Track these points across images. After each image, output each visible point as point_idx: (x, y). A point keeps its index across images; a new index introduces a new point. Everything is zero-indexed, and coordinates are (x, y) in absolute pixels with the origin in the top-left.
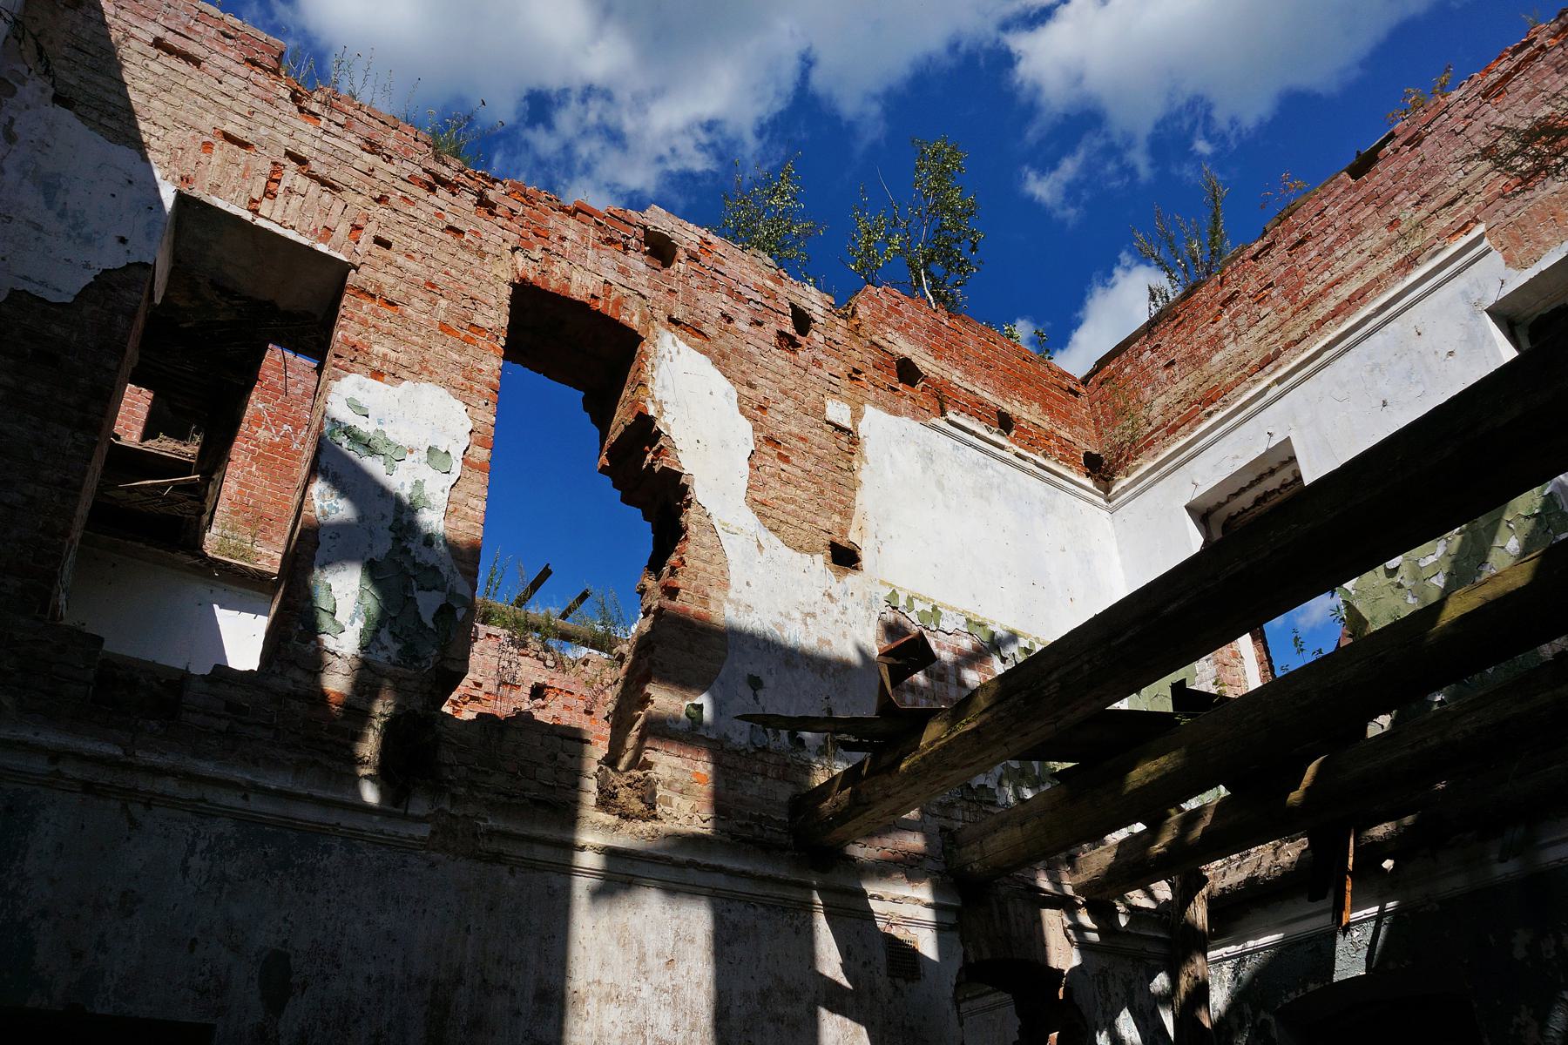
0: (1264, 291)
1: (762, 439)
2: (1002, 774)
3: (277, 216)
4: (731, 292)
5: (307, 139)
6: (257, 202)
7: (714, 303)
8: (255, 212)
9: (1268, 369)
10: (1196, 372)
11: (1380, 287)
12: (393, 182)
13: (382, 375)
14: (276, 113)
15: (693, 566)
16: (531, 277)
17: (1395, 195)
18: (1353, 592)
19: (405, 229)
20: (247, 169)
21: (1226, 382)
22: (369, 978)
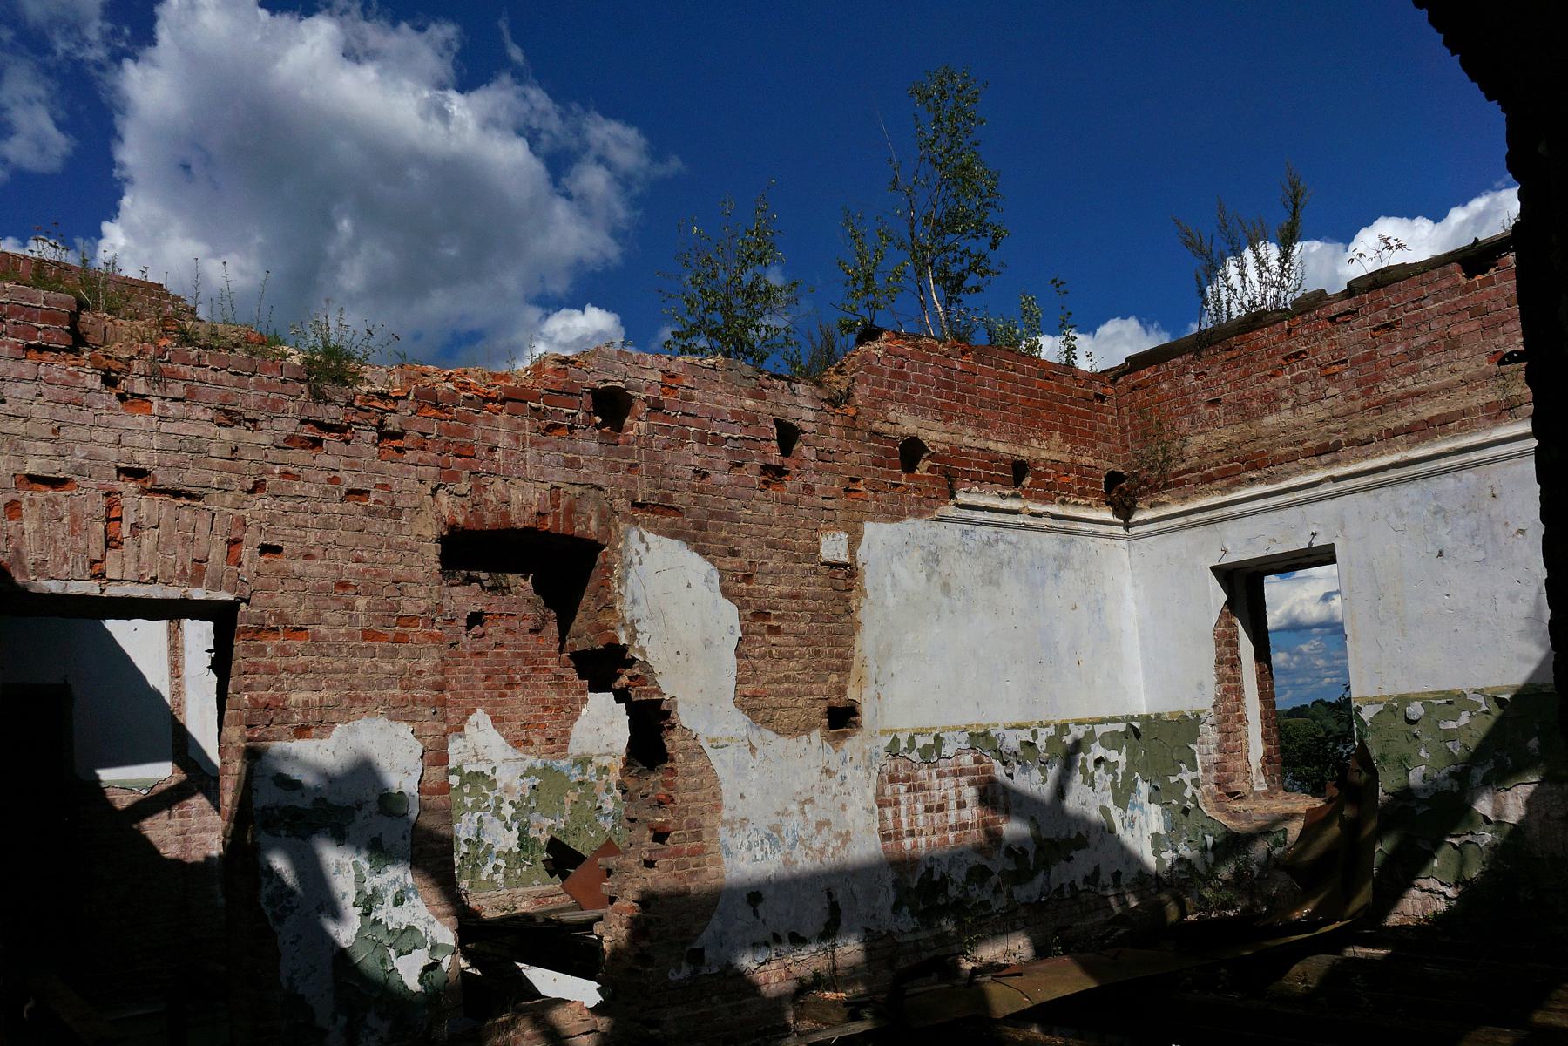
0: (1336, 367)
1: (749, 617)
2: (998, 883)
3: (131, 571)
4: (702, 438)
5: (140, 439)
6: (101, 562)
7: (684, 460)
8: (101, 575)
9: (1325, 459)
10: (1244, 425)
11: (1463, 423)
12: (266, 456)
13: (308, 728)
14: (88, 416)
15: (682, 800)
16: (460, 519)
17: (1506, 322)
18: (1369, 724)
19: (295, 518)
20: (74, 520)
21: (1276, 452)
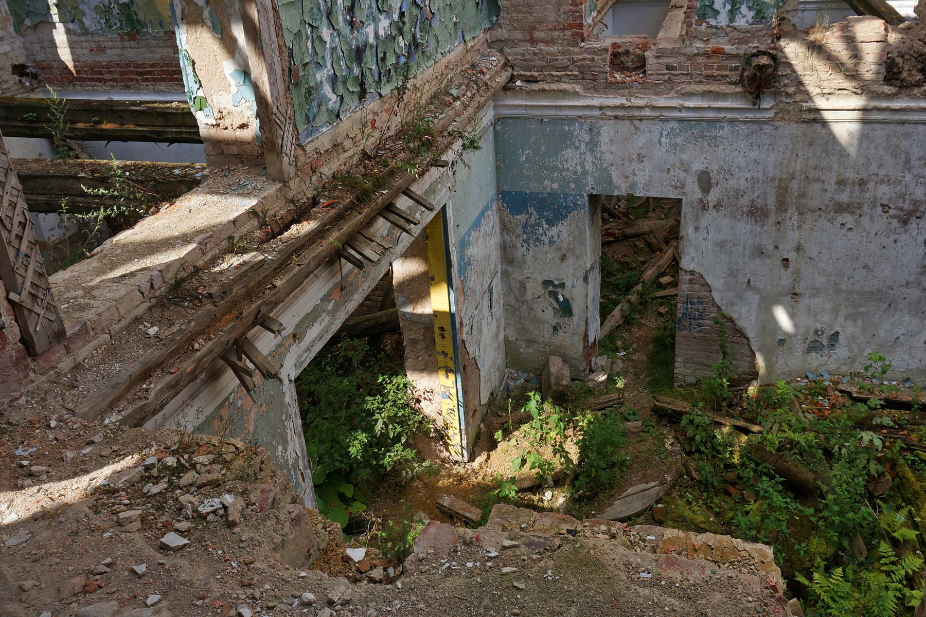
22: (747, 179)
